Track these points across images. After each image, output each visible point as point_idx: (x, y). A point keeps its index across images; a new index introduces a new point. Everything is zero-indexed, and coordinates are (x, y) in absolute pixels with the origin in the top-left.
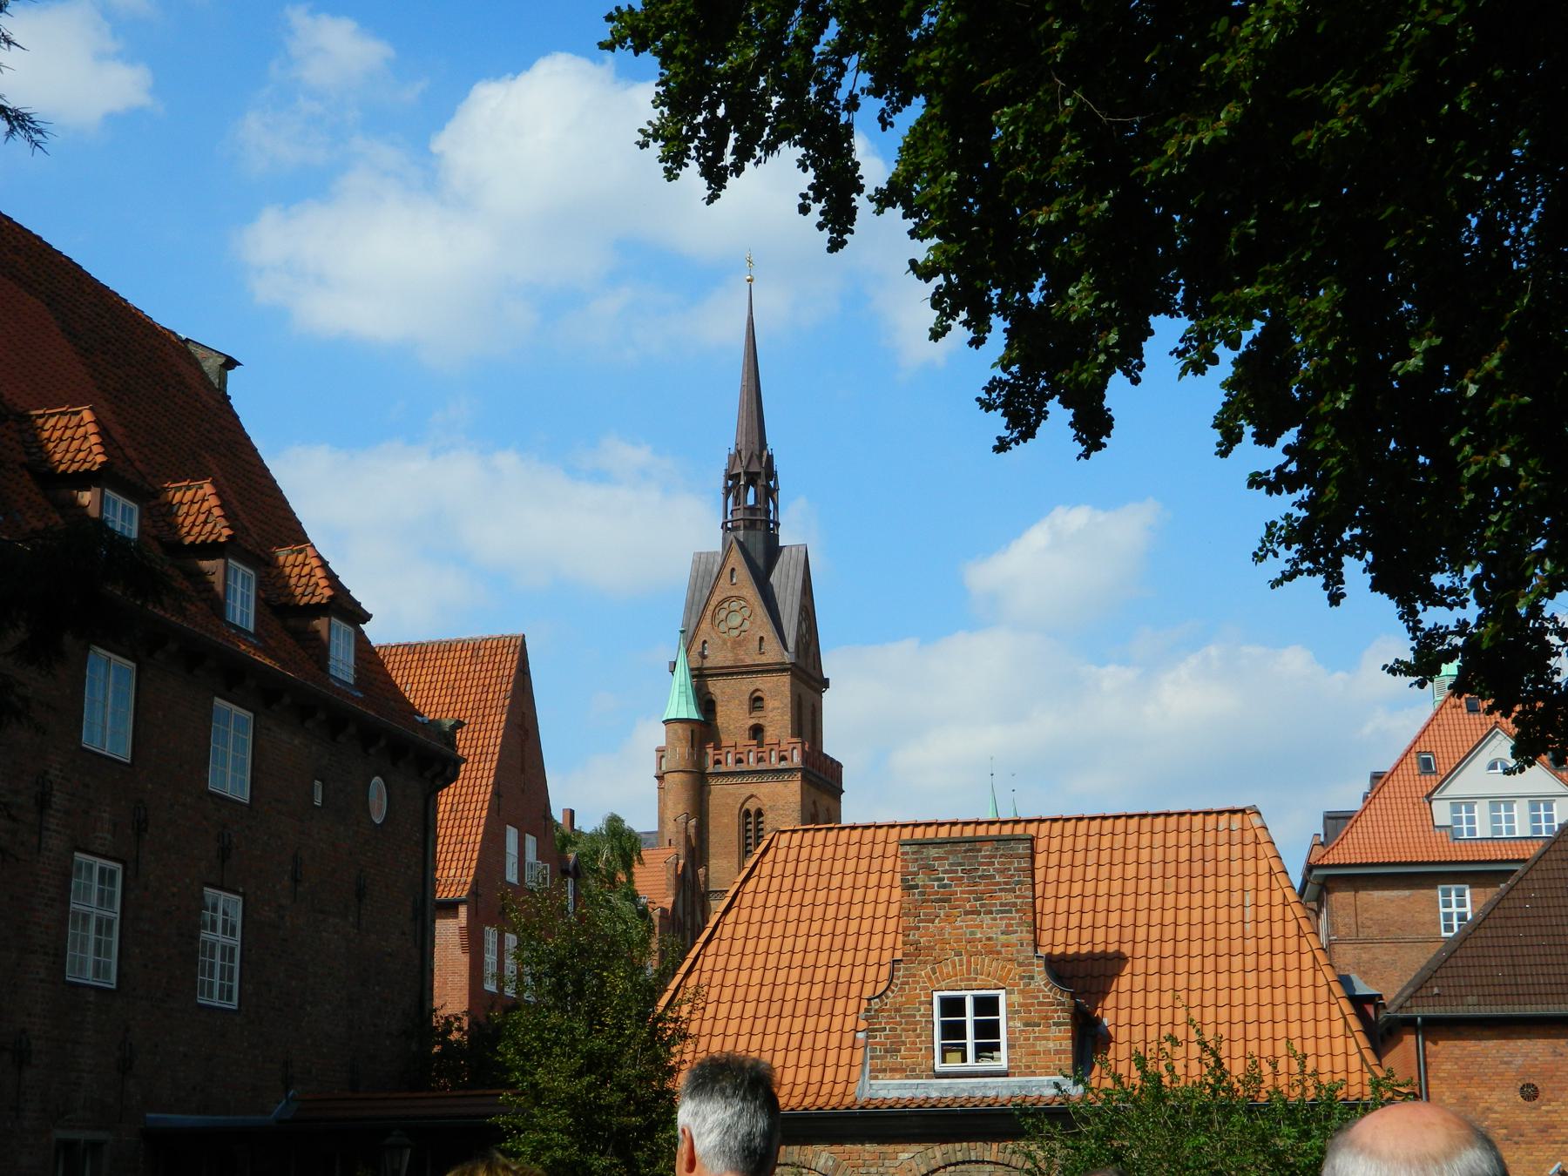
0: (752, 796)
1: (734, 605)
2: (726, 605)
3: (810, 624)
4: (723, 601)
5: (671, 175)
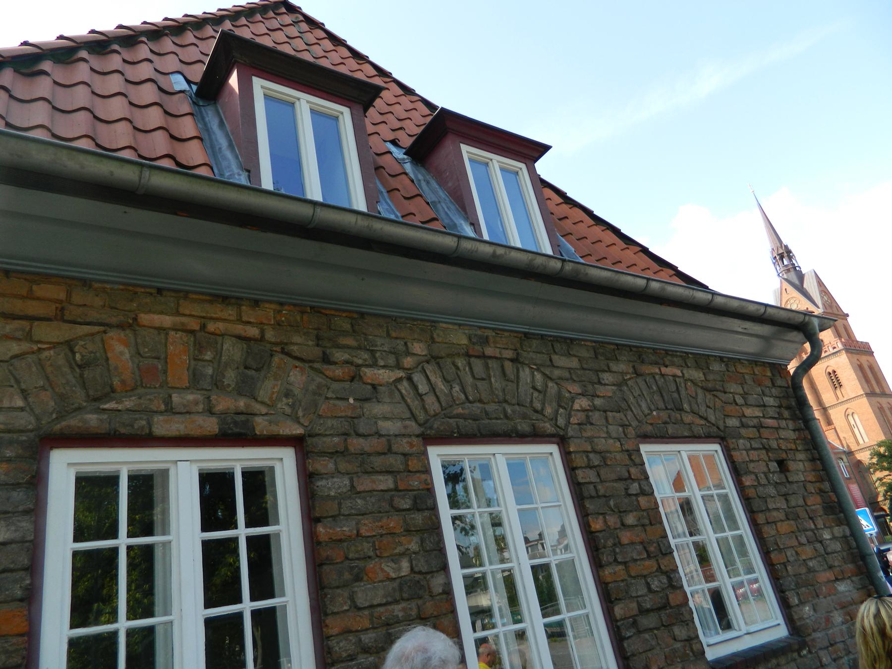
0: (828, 366)
1: (792, 301)
2: (788, 302)
3: (829, 297)
4: (787, 302)
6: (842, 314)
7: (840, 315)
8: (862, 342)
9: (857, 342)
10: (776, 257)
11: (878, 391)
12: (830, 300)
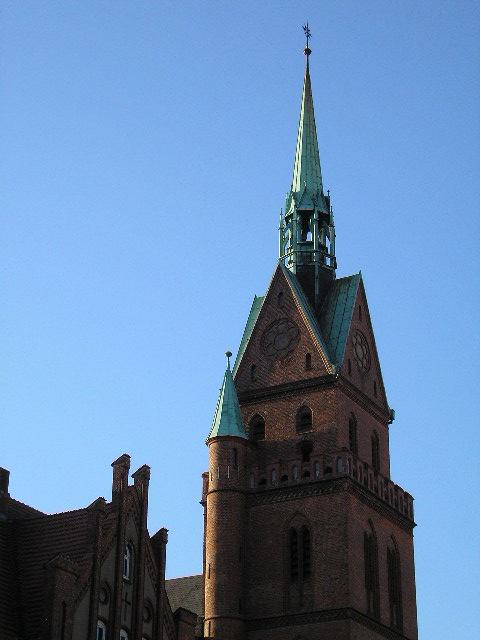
5: (162, 535)
6: (381, 405)
7: (379, 409)
8: (397, 488)
9: (388, 481)
10: (291, 216)
11: (385, 616)
12: (369, 362)
